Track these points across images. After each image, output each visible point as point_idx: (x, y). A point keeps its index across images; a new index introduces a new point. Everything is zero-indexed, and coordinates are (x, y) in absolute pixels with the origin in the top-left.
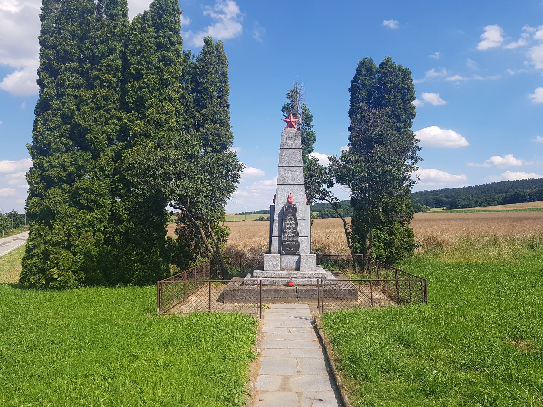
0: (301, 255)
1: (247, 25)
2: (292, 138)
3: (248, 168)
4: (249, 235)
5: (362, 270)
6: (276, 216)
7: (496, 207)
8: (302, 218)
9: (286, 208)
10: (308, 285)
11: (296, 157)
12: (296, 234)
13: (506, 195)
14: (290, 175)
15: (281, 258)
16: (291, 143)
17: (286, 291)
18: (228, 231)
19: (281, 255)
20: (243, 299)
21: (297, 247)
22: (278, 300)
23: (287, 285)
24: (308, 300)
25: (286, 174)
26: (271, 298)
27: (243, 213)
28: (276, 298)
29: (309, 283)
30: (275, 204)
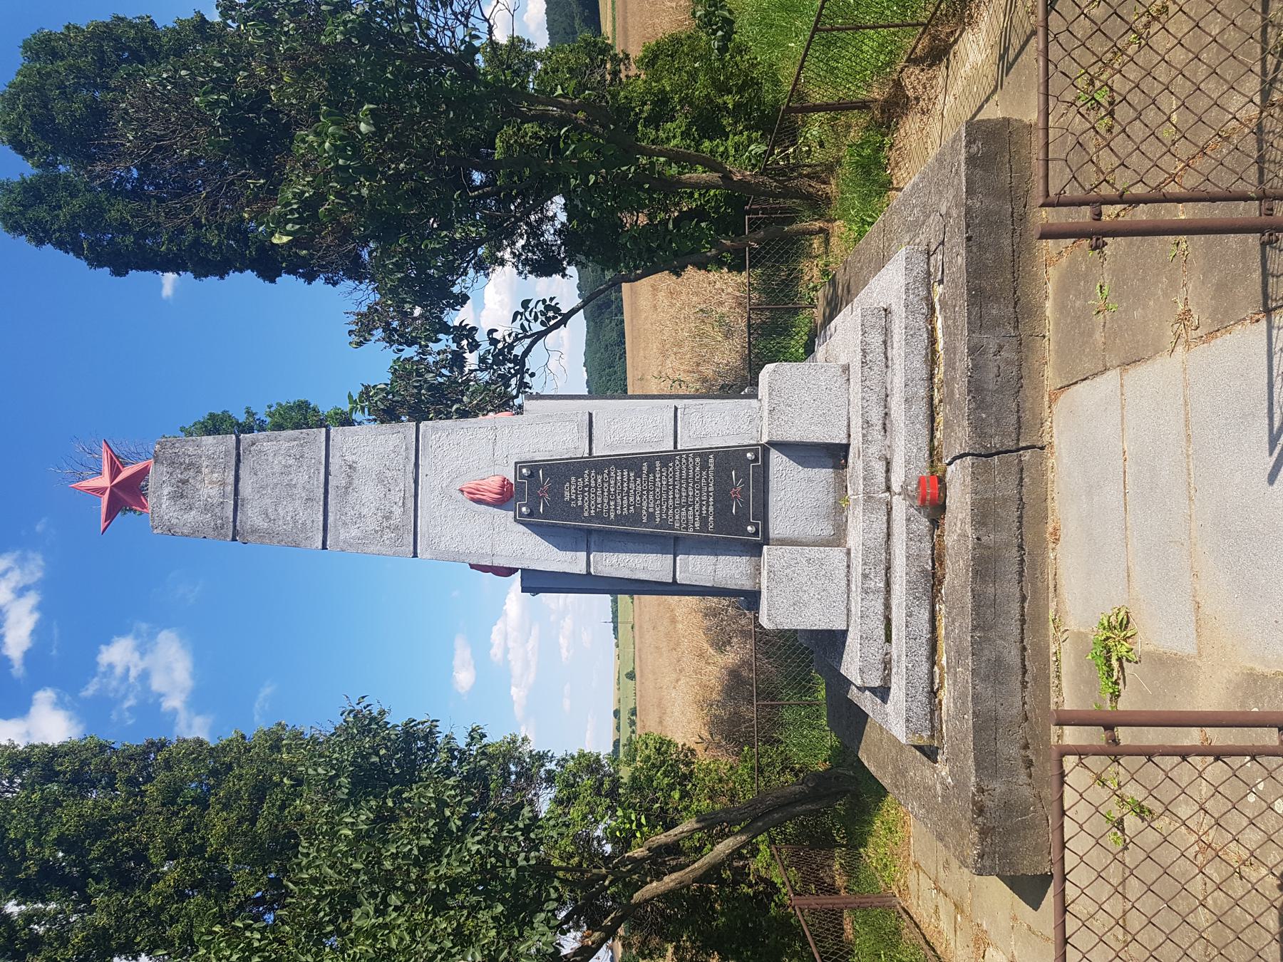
0: (765, 440)
1: (162, 620)
2: (185, 482)
3: (506, 615)
4: (666, 622)
5: (818, 204)
6: (572, 562)
7: (700, 867)
8: (586, 434)
9: (530, 515)
10: (931, 398)
11: (277, 463)
12: (664, 465)
13: (577, 19)
14: (368, 496)
15: (783, 542)
16: (210, 488)
17: (983, 515)
18: (651, 743)
19: (767, 541)
20: (1029, 764)
21: (728, 459)
22: (1033, 562)
23: (935, 508)
24: (1028, 391)
25: (365, 511)
26: (1023, 599)
27: (615, 629)
28: (1021, 573)
29: (922, 392)
30: (516, 570)
